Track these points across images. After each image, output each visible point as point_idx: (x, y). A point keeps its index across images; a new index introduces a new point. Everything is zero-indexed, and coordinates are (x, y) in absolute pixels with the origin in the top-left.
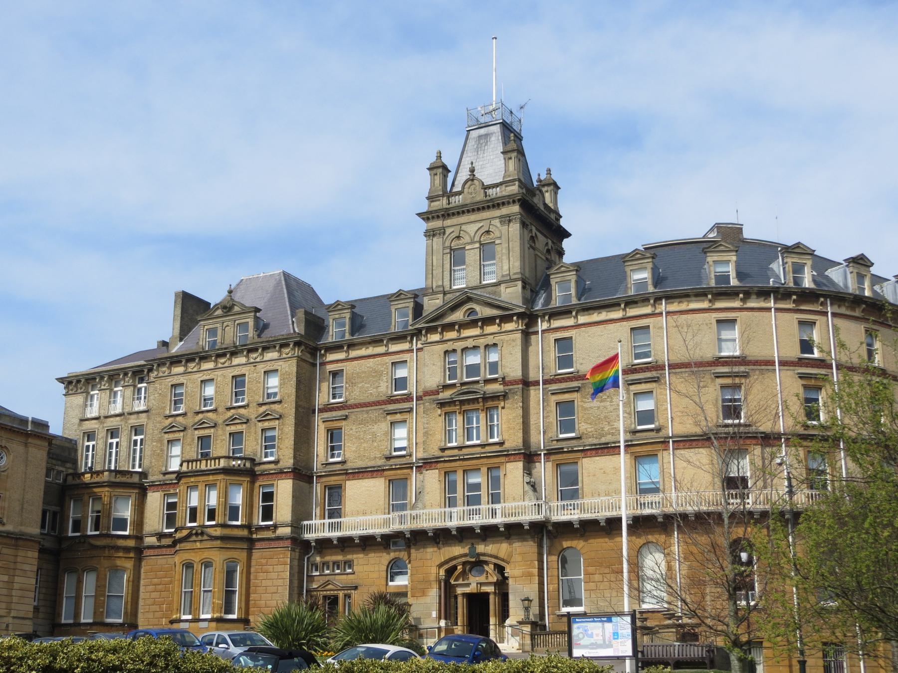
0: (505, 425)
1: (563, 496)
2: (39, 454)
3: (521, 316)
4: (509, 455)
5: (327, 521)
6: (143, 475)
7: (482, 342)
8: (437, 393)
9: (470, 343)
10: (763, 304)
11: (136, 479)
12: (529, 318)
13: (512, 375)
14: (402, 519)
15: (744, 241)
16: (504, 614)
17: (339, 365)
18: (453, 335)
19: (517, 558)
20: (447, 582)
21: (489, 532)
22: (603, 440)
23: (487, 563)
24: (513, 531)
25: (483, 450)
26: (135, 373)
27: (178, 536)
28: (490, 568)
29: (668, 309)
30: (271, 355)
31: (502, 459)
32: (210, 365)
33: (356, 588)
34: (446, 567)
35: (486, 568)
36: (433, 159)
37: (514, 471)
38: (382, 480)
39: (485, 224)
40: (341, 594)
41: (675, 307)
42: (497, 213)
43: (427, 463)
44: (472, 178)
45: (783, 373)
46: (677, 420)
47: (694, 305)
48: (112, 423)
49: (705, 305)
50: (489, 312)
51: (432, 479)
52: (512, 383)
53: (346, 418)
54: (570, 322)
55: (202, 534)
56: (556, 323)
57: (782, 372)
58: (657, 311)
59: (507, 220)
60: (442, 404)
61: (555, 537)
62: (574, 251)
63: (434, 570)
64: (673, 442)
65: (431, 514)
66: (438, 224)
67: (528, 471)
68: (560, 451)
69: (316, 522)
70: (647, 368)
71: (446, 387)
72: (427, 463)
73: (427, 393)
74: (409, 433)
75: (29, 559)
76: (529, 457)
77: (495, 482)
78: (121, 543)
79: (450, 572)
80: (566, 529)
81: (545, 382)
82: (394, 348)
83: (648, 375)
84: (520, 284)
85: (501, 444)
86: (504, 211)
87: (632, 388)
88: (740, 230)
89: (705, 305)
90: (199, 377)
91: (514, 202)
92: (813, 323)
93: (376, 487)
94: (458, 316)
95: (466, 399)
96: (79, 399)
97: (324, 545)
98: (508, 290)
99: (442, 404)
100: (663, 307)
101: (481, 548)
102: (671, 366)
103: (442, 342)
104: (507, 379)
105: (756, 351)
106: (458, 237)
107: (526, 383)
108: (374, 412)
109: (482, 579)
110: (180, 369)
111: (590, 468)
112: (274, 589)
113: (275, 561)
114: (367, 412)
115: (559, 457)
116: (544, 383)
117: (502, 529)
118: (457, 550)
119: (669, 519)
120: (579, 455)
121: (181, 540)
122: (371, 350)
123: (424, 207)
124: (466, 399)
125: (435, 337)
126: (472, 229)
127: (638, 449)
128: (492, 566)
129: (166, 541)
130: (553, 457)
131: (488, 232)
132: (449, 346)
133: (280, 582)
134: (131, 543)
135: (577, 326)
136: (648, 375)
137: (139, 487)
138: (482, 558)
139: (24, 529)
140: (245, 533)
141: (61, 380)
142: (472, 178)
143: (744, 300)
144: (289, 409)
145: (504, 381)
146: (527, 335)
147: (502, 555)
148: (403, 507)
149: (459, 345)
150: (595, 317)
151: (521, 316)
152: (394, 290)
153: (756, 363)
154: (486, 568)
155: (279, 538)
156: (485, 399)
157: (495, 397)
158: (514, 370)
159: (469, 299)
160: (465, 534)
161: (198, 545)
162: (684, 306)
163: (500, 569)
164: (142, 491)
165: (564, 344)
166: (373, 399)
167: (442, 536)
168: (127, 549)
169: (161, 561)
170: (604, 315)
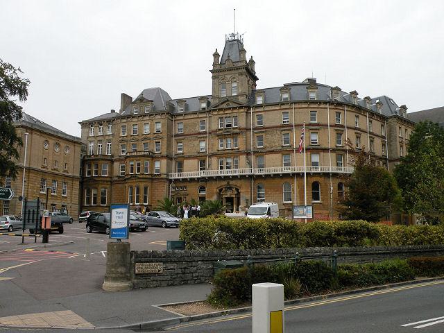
0: (241, 143)
1: (259, 166)
2: (78, 149)
3: (246, 107)
4: (241, 153)
5: (177, 173)
6: (112, 156)
7: (232, 115)
8: (216, 131)
9: (228, 115)
10: (326, 106)
11: (109, 158)
12: (248, 108)
15: (316, 84)
16: (238, 204)
20: (219, 194)
21: (235, 177)
22: (273, 149)
24: (243, 177)
26: (98, 123)
27: (126, 177)
28: (234, 189)
30: (158, 117)
32: (136, 120)
37: (243, 158)
41: (297, 106)
42: (237, 71)
43: (213, 155)
44: (228, 59)
45: (326, 122)
47: (303, 106)
49: (306, 106)
50: (235, 105)
51: (215, 160)
52: (243, 129)
54: (262, 110)
56: (257, 110)
59: (241, 74)
60: (218, 136)
62: (260, 85)
63: (215, 190)
65: (214, 172)
67: (247, 158)
68: (258, 152)
70: (287, 126)
71: (220, 130)
72: (213, 155)
73: (213, 132)
74: (206, 144)
75: (77, 185)
76: (248, 154)
77: (236, 162)
78: (105, 179)
79: (221, 190)
80: (260, 177)
81: (253, 129)
82: (201, 116)
83: (287, 128)
86: (240, 71)
88: (315, 81)
89: (306, 106)
92: (340, 113)
93: (195, 162)
94: (224, 106)
95: (227, 133)
96: (87, 130)
97: (177, 181)
99: (218, 136)
100: (293, 106)
101: (231, 183)
102: (330, 126)
105: (322, 122)
108: (194, 137)
110: (125, 120)
111: (294, 156)
118: (224, 183)
119: (294, 174)
121: (127, 179)
122: (192, 116)
125: (216, 113)
129: (121, 179)
132: (221, 116)
134: (108, 179)
136: (287, 128)
137: (111, 160)
139: (75, 174)
140: (150, 177)
141: (80, 123)
142: (228, 59)
144: (165, 135)
147: (238, 185)
148: (205, 169)
149: (225, 116)
150: (270, 108)
151: (246, 107)
153: (322, 125)
155: (162, 179)
156: (233, 134)
159: (228, 101)
160: (226, 178)
162: (300, 106)
163: (237, 190)
164: (112, 162)
165: (260, 117)
166: (193, 133)
167: (219, 178)
168: (107, 181)
169: (120, 186)
170: (273, 108)
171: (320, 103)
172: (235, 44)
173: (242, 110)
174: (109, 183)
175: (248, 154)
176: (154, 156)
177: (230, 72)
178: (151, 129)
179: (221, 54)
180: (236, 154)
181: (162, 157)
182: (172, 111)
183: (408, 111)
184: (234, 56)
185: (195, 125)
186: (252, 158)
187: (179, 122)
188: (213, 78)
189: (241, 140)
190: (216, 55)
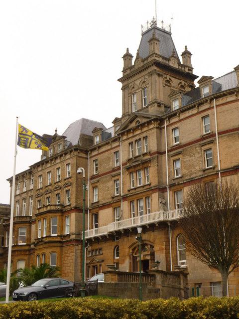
9: (137, 138)
13: (153, 150)
14: (119, 224)
17: (96, 157)
18: (131, 135)
19: (157, 241)
22: (192, 177)
23: (146, 244)
25: (144, 188)
29: (217, 104)
31: (150, 192)
33: (103, 261)
34: (132, 248)
35: (146, 247)
36: (125, 52)
37: (155, 196)
38: (111, 208)
39: (143, 78)
40: (98, 264)
41: (221, 101)
45: (220, 140)
46: (222, 162)
48: (24, 196)
50: (144, 120)
52: (154, 153)
53: (98, 181)
55: (42, 241)
57: (220, 140)
58: (212, 106)
61: (174, 229)
63: (127, 250)
64: (221, 173)
66: (126, 83)
69: (88, 231)
76: (162, 190)
81: (169, 151)
83: (209, 140)
84: (156, 105)
85: (150, 185)
86: (150, 70)
87: (203, 148)
90: (66, 163)
91: (152, 65)
94: (133, 125)
98: (152, 108)
103: (128, 139)
104: (151, 152)
106: (133, 87)
107: (160, 153)
108: (108, 177)
109: (146, 253)
112: (69, 265)
113: (70, 251)
114: (106, 177)
115: (175, 188)
116: (168, 152)
117: (157, 225)
120: (183, 185)
123: (121, 75)
124: (136, 165)
126: (138, 82)
127: (206, 179)
128: (149, 246)
130: (173, 188)
131: (144, 82)
133: (71, 261)
135: (180, 121)
138: (145, 242)
140: (59, 239)
143: (133, 133)
145: (150, 153)
146: (160, 128)
149: (133, 140)
151: (155, 120)
152: (209, 76)
154: (146, 247)
155: (71, 241)
157: (149, 161)
158: (154, 148)
161: (41, 247)
166: (108, 171)
171: (211, 100)
172: (155, 36)
173: (152, 126)
174: (27, 253)
175: (162, 190)
176: (64, 209)
177: (139, 76)
178: (36, 183)
179: (135, 56)
180: (145, 192)
181: (71, 210)
182: (88, 143)
183: (134, 53)
184: (159, 49)
185: (109, 159)
186: (168, 194)
187: (173, 127)
188: (123, 89)
189: (152, 170)
190: (127, 57)
